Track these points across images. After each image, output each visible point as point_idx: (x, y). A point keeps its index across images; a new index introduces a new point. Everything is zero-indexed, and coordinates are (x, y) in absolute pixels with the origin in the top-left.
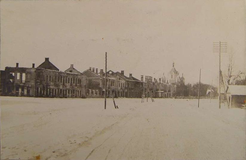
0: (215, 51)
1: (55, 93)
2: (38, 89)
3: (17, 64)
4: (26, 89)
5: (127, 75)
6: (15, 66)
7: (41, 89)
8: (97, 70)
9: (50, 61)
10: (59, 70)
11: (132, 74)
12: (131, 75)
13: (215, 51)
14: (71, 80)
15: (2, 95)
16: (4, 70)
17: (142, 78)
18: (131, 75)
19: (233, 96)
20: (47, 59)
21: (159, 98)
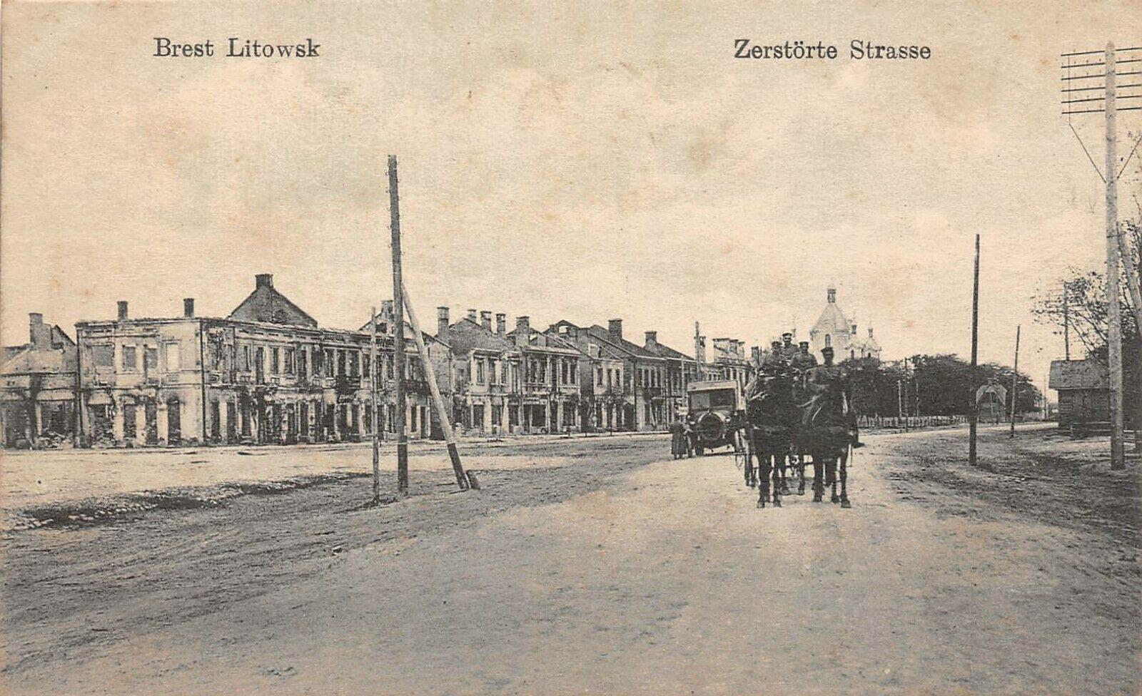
0: (1074, 107)
1: (415, 417)
2: (216, 405)
3: (123, 306)
4: (162, 410)
5: (634, 334)
6: (115, 317)
7: (230, 405)
8: (500, 317)
9: (277, 287)
10: (315, 324)
11: (269, 276)
12: (651, 336)
13: (1074, 107)
14: (653, 377)
15: (14, 443)
16: (1057, 392)
17: (701, 343)
18: (651, 336)
19: (218, 402)
20: (263, 281)
21: (279, 442)
